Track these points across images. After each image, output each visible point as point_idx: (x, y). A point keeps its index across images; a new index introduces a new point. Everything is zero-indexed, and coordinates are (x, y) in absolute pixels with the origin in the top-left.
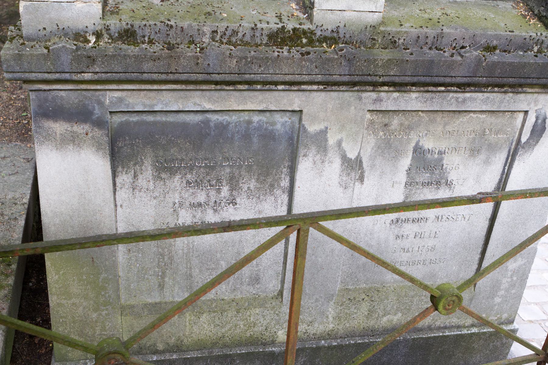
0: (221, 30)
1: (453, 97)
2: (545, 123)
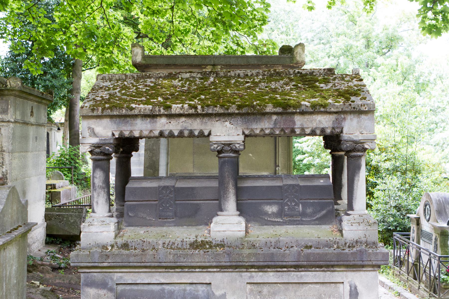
0: (167, 243)
1: (294, 275)
2: (357, 290)
